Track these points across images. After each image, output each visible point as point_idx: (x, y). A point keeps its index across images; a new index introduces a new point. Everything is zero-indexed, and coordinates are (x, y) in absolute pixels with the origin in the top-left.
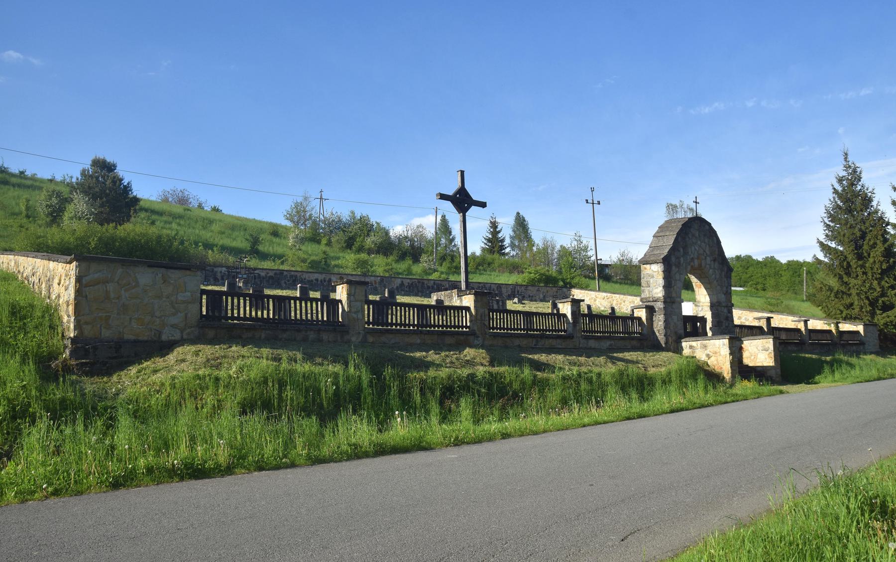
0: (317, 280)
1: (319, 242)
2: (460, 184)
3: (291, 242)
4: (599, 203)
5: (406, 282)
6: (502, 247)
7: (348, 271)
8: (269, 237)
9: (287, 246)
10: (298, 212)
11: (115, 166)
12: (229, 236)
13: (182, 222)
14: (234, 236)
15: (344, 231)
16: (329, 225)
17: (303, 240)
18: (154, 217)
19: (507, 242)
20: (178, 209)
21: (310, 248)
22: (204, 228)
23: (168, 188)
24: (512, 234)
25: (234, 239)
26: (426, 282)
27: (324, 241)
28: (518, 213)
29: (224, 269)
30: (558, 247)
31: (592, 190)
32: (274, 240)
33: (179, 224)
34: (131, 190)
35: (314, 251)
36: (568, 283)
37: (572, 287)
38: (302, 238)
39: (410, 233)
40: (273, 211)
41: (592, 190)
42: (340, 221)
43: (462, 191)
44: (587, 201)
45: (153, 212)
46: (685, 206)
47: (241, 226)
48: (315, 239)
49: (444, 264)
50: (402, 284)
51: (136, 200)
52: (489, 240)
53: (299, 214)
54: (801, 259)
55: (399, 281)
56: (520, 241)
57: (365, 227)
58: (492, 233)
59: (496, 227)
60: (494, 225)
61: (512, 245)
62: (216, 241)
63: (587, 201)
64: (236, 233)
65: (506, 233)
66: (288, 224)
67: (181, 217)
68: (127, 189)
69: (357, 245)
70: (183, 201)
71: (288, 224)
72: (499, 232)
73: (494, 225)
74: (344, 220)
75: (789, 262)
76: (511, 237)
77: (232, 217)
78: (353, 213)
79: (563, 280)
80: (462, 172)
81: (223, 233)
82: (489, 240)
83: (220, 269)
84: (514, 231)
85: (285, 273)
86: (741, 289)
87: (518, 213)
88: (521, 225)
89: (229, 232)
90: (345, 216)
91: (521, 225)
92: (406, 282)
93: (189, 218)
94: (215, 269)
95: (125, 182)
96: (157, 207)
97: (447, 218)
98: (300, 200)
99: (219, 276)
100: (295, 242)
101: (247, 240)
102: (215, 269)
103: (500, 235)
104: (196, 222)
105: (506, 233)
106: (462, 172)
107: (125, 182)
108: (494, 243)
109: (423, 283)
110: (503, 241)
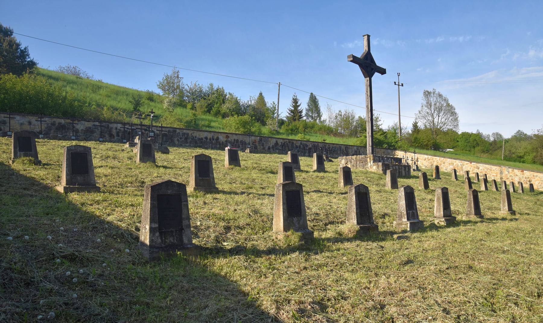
0: (206, 138)
1: (185, 106)
2: (366, 48)
3: (165, 105)
4: (402, 85)
5: (280, 142)
6: (300, 117)
7: (233, 131)
8: (147, 101)
9: (162, 109)
10: (168, 83)
11: (12, 33)
12: (115, 99)
13: (75, 86)
14: (119, 100)
15: (205, 99)
16: (192, 94)
17: (175, 105)
18: (51, 81)
19: (304, 113)
20: (73, 78)
21: (179, 111)
22: (94, 92)
23: (64, 65)
24: (307, 107)
25: (119, 102)
26: (295, 142)
27: (189, 106)
28: (312, 94)
29: (119, 126)
30: (357, 117)
31: (399, 75)
32: (151, 104)
33: (72, 88)
34: (28, 55)
35: (186, 114)
36: (392, 146)
37: (395, 149)
38: (175, 103)
39: (253, 102)
40: (147, 81)
41: (399, 75)
42: (201, 91)
43: (368, 56)
44: (395, 83)
45: (50, 77)
46: (437, 92)
47: (123, 92)
48: (181, 104)
49: (283, 127)
50: (277, 143)
51: (32, 64)
52: (292, 111)
53: (171, 85)
54: (470, 131)
55: (274, 141)
56: (312, 113)
57: (220, 96)
58: (294, 107)
59: (297, 103)
60: (295, 101)
61: (307, 115)
62: (104, 103)
63: (395, 83)
64: (119, 98)
65: (304, 106)
66: (161, 93)
67: (74, 83)
68: (24, 54)
69: (214, 110)
70: (77, 75)
71: (161, 93)
72: (299, 106)
73: (295, 101)
74: (204, 90)
75: (463, 133)
76: (307, 110)
77: (114, 86)
78: (212, 85)
79: (388, 143)
80: (369, 36)
81: (109, 97)
82: (292, 111)
83: (115, 125)
84: (308, 106)
85: (178, 131)
86: (451, 150)
87: (312, 94)
88: (314, 101)
89: (114, 96)
90: (205, 88)
91: (314, 101)
92: (280, 142)
93: (81, 84)
94: (111, 125)
95: (22, 47)
96: (54, 75)
97: (263, 95)
98: (170, 73)
99: (114, 132)
100: (169, 105)
101: (130, 102)
102: (111, 125)
103: (299, 108)
104: (87, 87)
105: (304, 106)
106: (369, 36)
107: (22, 47)
108: (295, 113)
109: (293, 143)
110: (301, 112)
